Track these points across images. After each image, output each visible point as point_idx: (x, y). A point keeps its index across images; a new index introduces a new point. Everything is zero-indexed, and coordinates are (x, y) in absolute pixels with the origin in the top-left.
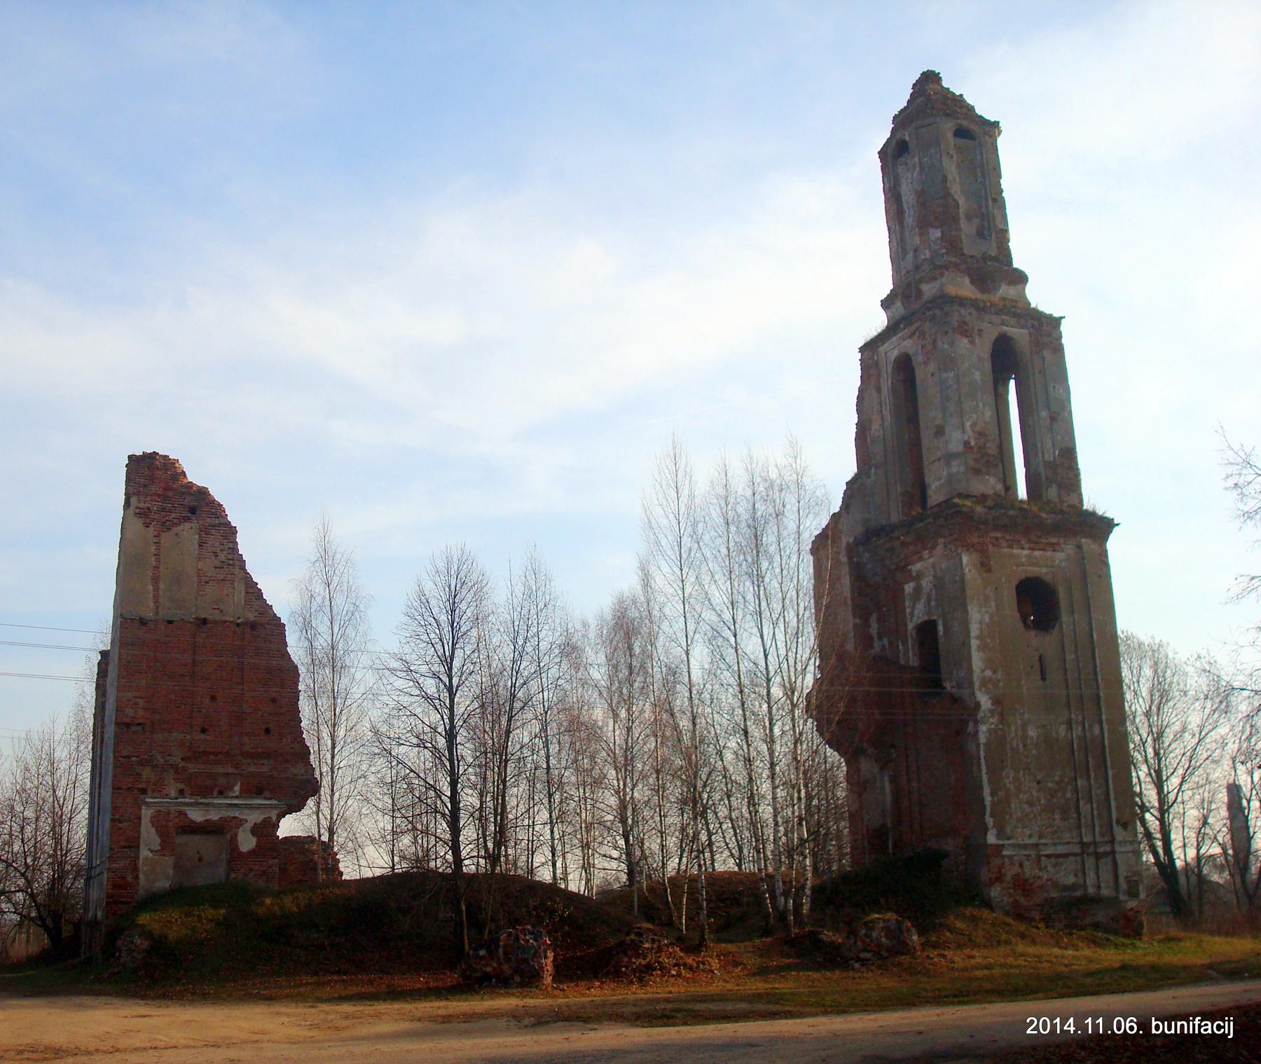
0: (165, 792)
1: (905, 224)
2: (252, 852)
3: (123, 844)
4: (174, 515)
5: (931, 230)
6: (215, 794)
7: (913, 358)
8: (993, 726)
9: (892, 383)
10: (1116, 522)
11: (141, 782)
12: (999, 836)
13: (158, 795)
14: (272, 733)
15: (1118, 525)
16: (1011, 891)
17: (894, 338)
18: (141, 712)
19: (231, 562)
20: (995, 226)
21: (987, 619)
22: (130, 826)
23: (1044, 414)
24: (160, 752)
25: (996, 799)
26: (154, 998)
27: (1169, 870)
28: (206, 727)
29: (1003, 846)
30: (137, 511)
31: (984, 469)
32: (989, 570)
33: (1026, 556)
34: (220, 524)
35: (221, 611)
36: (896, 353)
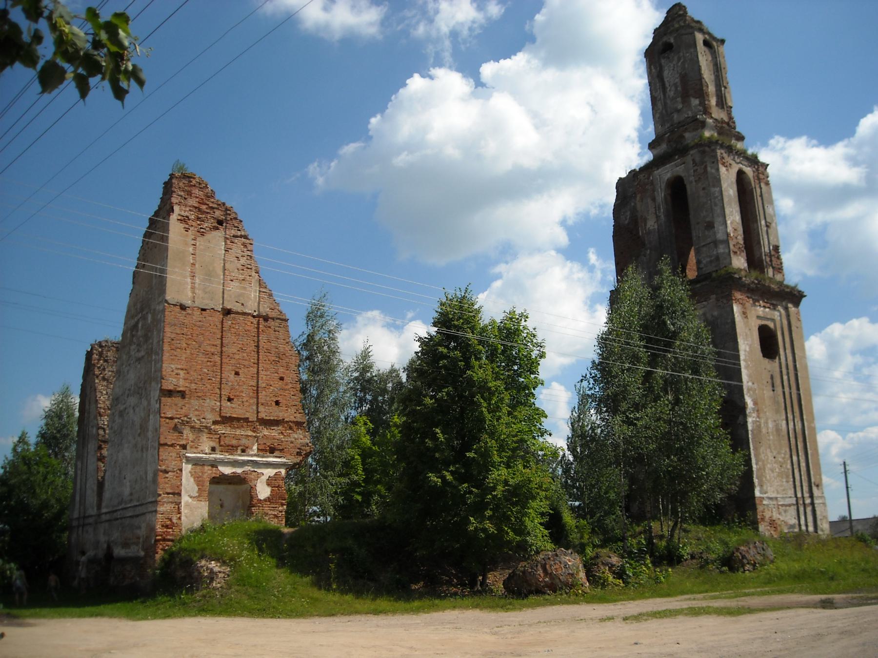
0: (201, 448)
1: (667, 96)
2: (268, 500)
3: (169, 491)
4: (206, 225)
5: (692, 100)
6: (239, 452)
7: (684, 178)
8: (754, 419)
9: (665, 195)
10: (805, 294)
11: (183, 439)
12: (761, 493)
13: (195, 451)
14: (281, 405)
15: (805, 296)
16: (769, 528)
17: (668, 166)
18: (181, 382)
19: (249, 266)
20: (726, 103)
21: (748, 349)
22: (174, 476)
23: (763, 222)
24: (196, 416)
25: (758, 467)
26: (486, 608)
27: (8, 572)
28: (232, 397)
29: (763, 498)
30: (179, 218)
31: (738, 253)
32: (746, 317)
33: (762, 311)
34: (241, 235)
35: (243, 304)
36: (669, 175)
